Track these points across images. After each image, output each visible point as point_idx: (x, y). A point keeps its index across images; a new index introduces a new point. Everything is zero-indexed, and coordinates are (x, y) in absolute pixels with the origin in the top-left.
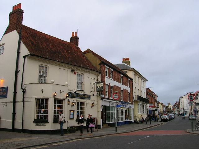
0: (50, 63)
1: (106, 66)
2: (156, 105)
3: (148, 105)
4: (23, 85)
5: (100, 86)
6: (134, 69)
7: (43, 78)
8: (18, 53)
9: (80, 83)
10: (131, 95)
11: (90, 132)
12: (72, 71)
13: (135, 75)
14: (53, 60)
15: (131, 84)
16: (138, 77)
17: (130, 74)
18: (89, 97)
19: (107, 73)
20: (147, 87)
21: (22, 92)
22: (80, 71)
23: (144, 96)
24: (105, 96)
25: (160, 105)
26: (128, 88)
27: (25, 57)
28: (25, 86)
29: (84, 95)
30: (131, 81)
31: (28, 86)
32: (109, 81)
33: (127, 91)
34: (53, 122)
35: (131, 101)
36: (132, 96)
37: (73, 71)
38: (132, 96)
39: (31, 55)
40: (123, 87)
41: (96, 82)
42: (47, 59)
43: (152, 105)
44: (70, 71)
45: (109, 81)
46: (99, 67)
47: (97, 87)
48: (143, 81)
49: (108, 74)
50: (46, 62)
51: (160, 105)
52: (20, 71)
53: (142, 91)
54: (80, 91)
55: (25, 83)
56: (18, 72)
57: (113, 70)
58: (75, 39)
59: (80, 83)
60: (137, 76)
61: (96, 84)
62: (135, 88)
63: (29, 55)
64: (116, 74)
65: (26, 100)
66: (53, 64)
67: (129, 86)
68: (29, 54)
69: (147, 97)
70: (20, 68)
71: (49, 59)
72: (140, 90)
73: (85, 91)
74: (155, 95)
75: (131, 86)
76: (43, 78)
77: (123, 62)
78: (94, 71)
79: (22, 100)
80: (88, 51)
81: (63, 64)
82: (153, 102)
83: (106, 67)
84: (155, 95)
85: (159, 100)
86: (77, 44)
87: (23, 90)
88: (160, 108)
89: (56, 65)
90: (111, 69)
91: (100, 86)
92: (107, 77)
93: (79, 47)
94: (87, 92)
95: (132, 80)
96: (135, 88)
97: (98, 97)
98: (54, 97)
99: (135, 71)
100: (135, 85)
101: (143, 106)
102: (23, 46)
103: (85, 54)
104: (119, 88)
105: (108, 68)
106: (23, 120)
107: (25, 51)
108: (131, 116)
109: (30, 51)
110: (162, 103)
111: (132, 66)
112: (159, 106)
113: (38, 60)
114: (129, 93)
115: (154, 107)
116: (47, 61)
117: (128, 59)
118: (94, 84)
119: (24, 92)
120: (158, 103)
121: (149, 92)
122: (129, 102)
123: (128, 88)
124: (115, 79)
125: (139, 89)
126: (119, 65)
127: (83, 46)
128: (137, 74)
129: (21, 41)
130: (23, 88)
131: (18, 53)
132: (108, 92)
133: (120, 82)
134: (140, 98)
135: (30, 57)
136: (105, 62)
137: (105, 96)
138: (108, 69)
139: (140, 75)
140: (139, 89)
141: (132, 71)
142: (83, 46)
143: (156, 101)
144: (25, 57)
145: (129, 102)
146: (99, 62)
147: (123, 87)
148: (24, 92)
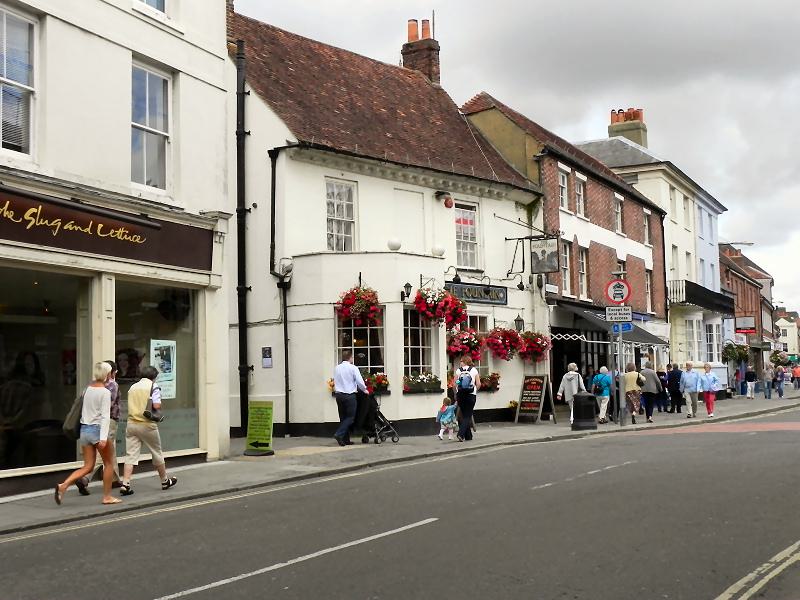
0: (361, 171)
1: (561, 165)
2: (767, 324)
3: (730, 324)
4: (277, 261)
5: (544, 252)
6: (668, 164)
7: (341, 238)
8: (242, 135)
9: (467, 241)
10: (658, 277)
11: (452, 436)
12: (439, 195)
13: (672, 189)
14: (373, 159)
15: (656, 231)
16: (686, 198)
17: (654, 188)
18: (501, 295)
19: (565, 192)
20: (726, 239)
21: (279, 285)
22: (464, 191)
23: (713, 283)
24: (560, 290)
25: (782, 323)
26: (644, 253)
27: (274, 154)
28: (287, 263)
29: (487, 289)
30: (656, 218)
31: (298, 265)
32: (576, 228)
33: (642, 262)
34: (405, 393)
35: (660, 306)
36: (659, 286)
37: (443, 193)
38: (659, 286)
39: (302, 145)
40: (626, 247)
41: (526, 232)
42: (355, 155)
43: (750, 322)
44: (430, 193)
45: (576, 228)
46: (532, 172)
47: (533, 255)
48: (705, 214)
49: (569, 197)
50: (349, 167)
51: (782, 323)
52: (255, 206)
53: (702, 260)
54: (470, 274)
55: (286, 250)
56: (249, 210)
57: (585, 178)
58: (422, 53)
59: (467, 241)
60: (679, 195)
61: (527, 242)
62: (674, 247)
63: (290, 145)
64: (598, 193)
65: (292, 314)
66: (372, 173)
67: (646, 243)
68: (294, 140)
69: (726, 288)
70: (258, 192)
71: (361, 156)
72: (692, 256)
73: (486, 273)
74: (762, 274)
75: (658, 242)
76: (341, 238)
77: (612, 132)
78: (520, 189)
79: (277, 313)
80: (483, 104)
81: (410, 169)
82: (752, 306)
83: (578, 179)
84: (761, 277)
85: (778, 297)
86: (433, 74)
87: (281, 278)
88: (782, 339)
89: (383, 175)
90: (579, 175)
91: (544, 252)
92: (565, 208)
93: (445, 83)
94: (494, 276)
95: (661, 213)
96: (674, 247)
97: (537, 296)
98: (403, 299)
99: (677, 177)
100: (672, 232)
101: (709, 328)
102: (255, 103)
103: (473, 119)
104: (611, 252)
105: (569, 170)
106: (287, 391)
107: (269, 128)
108: (22, 310)
109: (295, 131)
110: (795, 314)
111: (656, 147)
112: (777, 328)
113: (324, 163)
114: (648, 271)
115: (756, 330)
116: (355, 164)
117: (634, 115)
118: (520, 244)
119: (284, 287)
120: (776, 313)
121: (732, 263)
122: (649, 311)
123: (644, 253)
124: (591, 215)
125: (688, 254)
126: (598, 145)
127: (459, 83)
128: (681, 185)
129: (248, 88)
130: (277, 270)
131: (242, 135)
132: (588, 276)
133: (613, 229)
134: (697, 294)
135: (296, 152)
136: (554, 146)
137: (560, 290)
138: (568, 174)
139: (692, 189)
140: (688, 254)
141: (661, 174)
142: (459, 83)
143: (764, 303)
144: (274, 154)
145: (649, 311)
146: (533, 149)
147: (626, 247)
148: (284, 287)
